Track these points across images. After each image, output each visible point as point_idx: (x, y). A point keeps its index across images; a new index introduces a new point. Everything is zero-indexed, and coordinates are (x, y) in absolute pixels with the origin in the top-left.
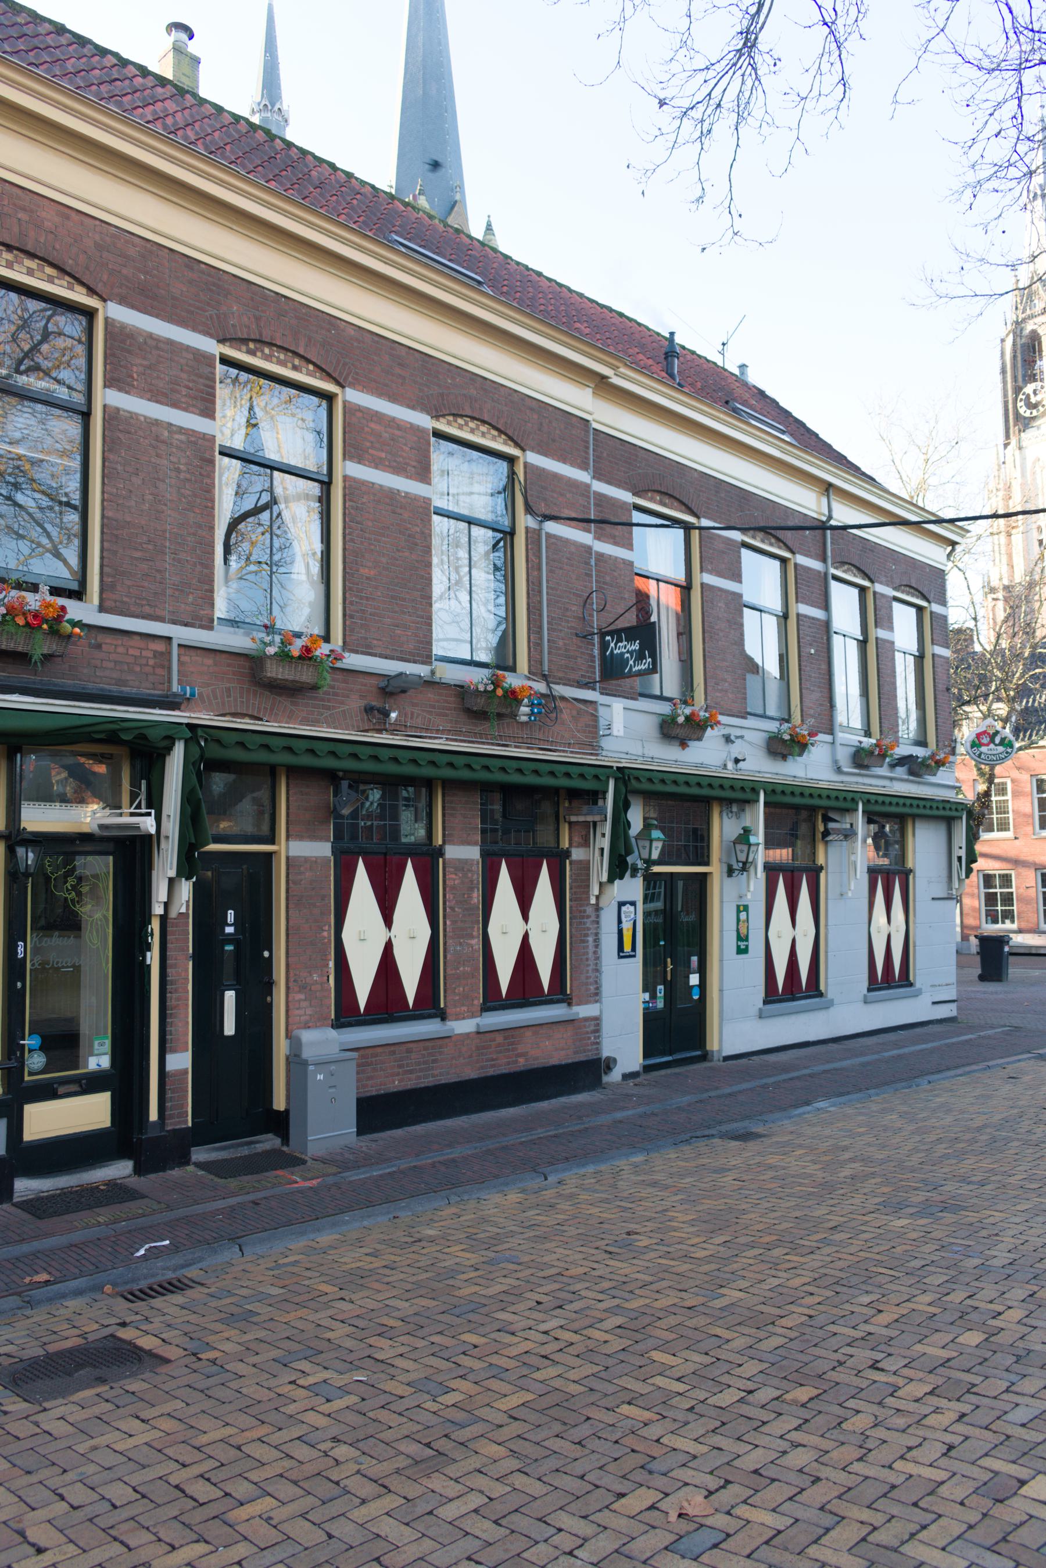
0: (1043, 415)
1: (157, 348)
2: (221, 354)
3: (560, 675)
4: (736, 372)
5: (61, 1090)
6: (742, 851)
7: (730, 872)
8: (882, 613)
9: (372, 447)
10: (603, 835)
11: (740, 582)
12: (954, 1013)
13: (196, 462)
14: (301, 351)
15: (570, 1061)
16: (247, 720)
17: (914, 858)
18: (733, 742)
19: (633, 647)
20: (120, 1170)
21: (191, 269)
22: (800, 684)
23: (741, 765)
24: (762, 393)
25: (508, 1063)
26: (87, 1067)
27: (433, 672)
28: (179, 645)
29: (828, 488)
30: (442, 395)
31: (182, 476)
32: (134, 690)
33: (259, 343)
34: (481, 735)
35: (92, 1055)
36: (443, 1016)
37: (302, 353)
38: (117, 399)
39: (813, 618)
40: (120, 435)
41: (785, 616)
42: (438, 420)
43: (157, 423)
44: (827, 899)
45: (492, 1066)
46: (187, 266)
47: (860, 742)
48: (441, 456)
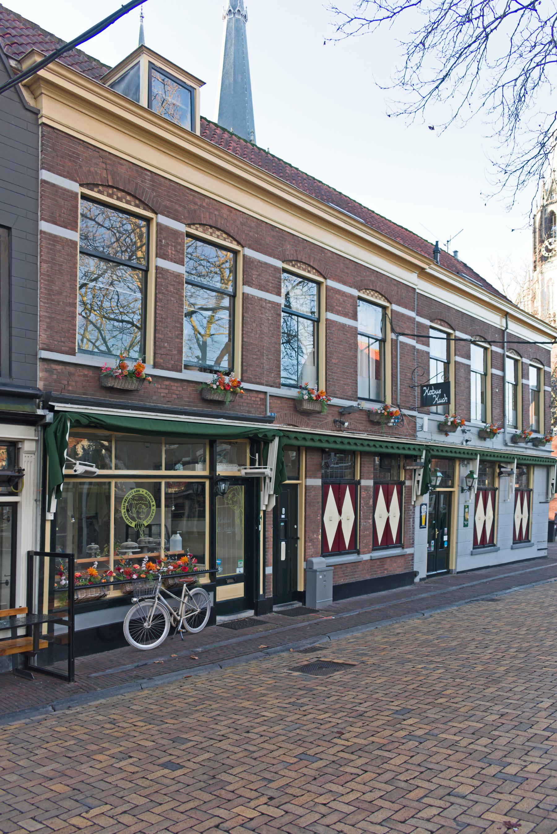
0: (555, 255)
1: (261, 266)
2: (82, 193)
3: (403, 405)
4: (453, 254)
5: (228, 581)
6: (469, 481)
7: (463, 490)
8: (525, 372)
9: (337, 305)
10: (419, 475)
11: (470, 360)
12: (546, 554)
13: (275, 316)
14: (311, 264)
15: (403, 572)
16: (291, 427)
17: (533, 484)
18: (466, 433)
19: (438, 393)
20: (250, 613)
21: (273, 230)
22: (492, 406)
23: (468, 443)
24: (465, 265)
25: (381, 573)
26: (236, 572)
27: (359, 405)
28: (270, 395)
29: (506, 315)
30: (362, 280)
31: (270, 322)
32: (254, 415)
33: (296, 261)
34: (375, 432)
35: (238, 567)
36: (358, 553)
37: (312, 265)
38: (248, 290)
39: (498, 375)
40: (249, 305)
41: (485, 375)
42: (190, 227)
43: (261, 299)
44: (498, 503)
45: (375, 574)
46: (272, 229)
47: (516, 432)
48: (362, 307)
